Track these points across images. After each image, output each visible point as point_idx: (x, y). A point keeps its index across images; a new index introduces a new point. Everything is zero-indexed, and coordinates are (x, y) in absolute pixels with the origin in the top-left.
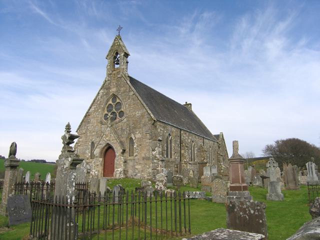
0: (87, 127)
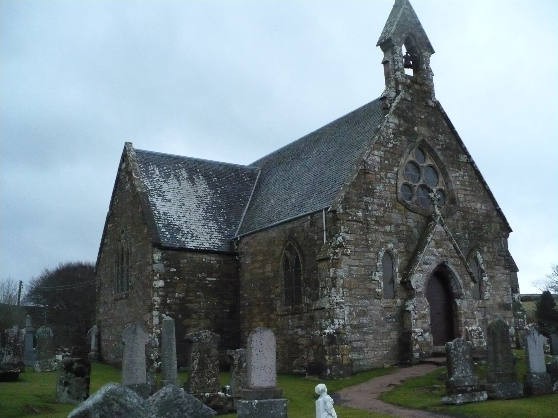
0: (367, 204)
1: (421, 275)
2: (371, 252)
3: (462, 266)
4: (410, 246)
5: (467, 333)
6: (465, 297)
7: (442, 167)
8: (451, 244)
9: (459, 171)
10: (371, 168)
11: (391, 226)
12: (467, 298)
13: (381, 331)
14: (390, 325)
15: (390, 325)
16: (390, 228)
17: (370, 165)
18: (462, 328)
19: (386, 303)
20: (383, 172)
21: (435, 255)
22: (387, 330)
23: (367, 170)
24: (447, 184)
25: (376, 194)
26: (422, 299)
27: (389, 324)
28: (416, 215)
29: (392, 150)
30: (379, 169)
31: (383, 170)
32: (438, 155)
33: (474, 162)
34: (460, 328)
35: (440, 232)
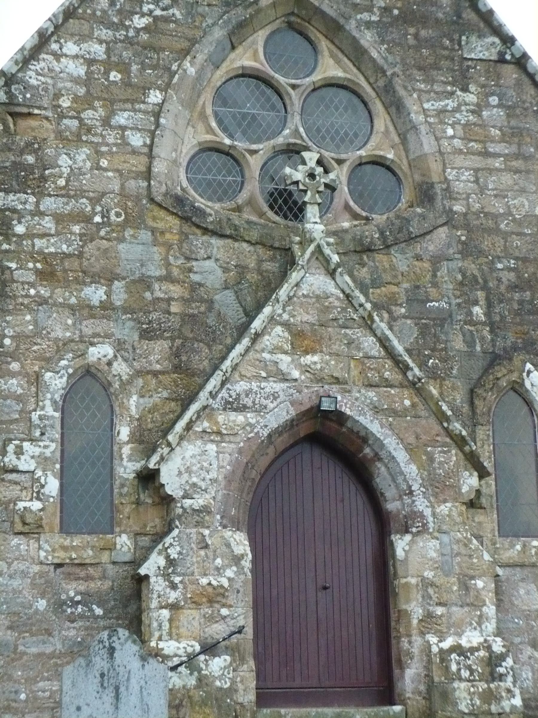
1: (212, 448)
2: (13, 375)
3: (423, 413)
4: (197, 352)
5: (430, 661)
6: (431, 525)
7: (381, 83)
8: (372, 339)
9: (459, 93)
10: (41, 97)
11: (109, 286)
12: (440, 531)
13: (34, 650)
14: (78, 630)
15: (78, 630)
16: (108, 294)
17: (37, 88)
18: (410, 642)
19: (65, 548)
20: (95, 109)
21: (284, 378)
22: (59, 646)
23: (19, 105)
24: (404, 141)
25: (54, 183)
26: (206, 532)
27: (75, 625)
28: (236, 244)
29: (145, 37)
30: (76, 99)
31: (97, 104)
32: (362, 42)
33: (529, 58)
34: (404, 641)
35: (318, 297)
